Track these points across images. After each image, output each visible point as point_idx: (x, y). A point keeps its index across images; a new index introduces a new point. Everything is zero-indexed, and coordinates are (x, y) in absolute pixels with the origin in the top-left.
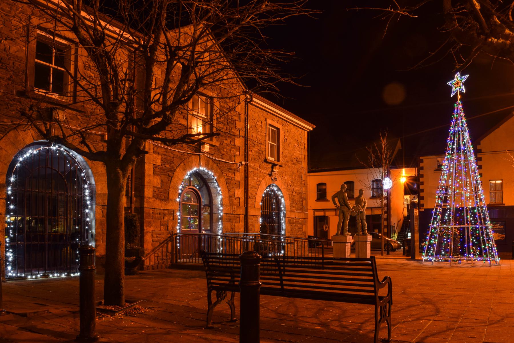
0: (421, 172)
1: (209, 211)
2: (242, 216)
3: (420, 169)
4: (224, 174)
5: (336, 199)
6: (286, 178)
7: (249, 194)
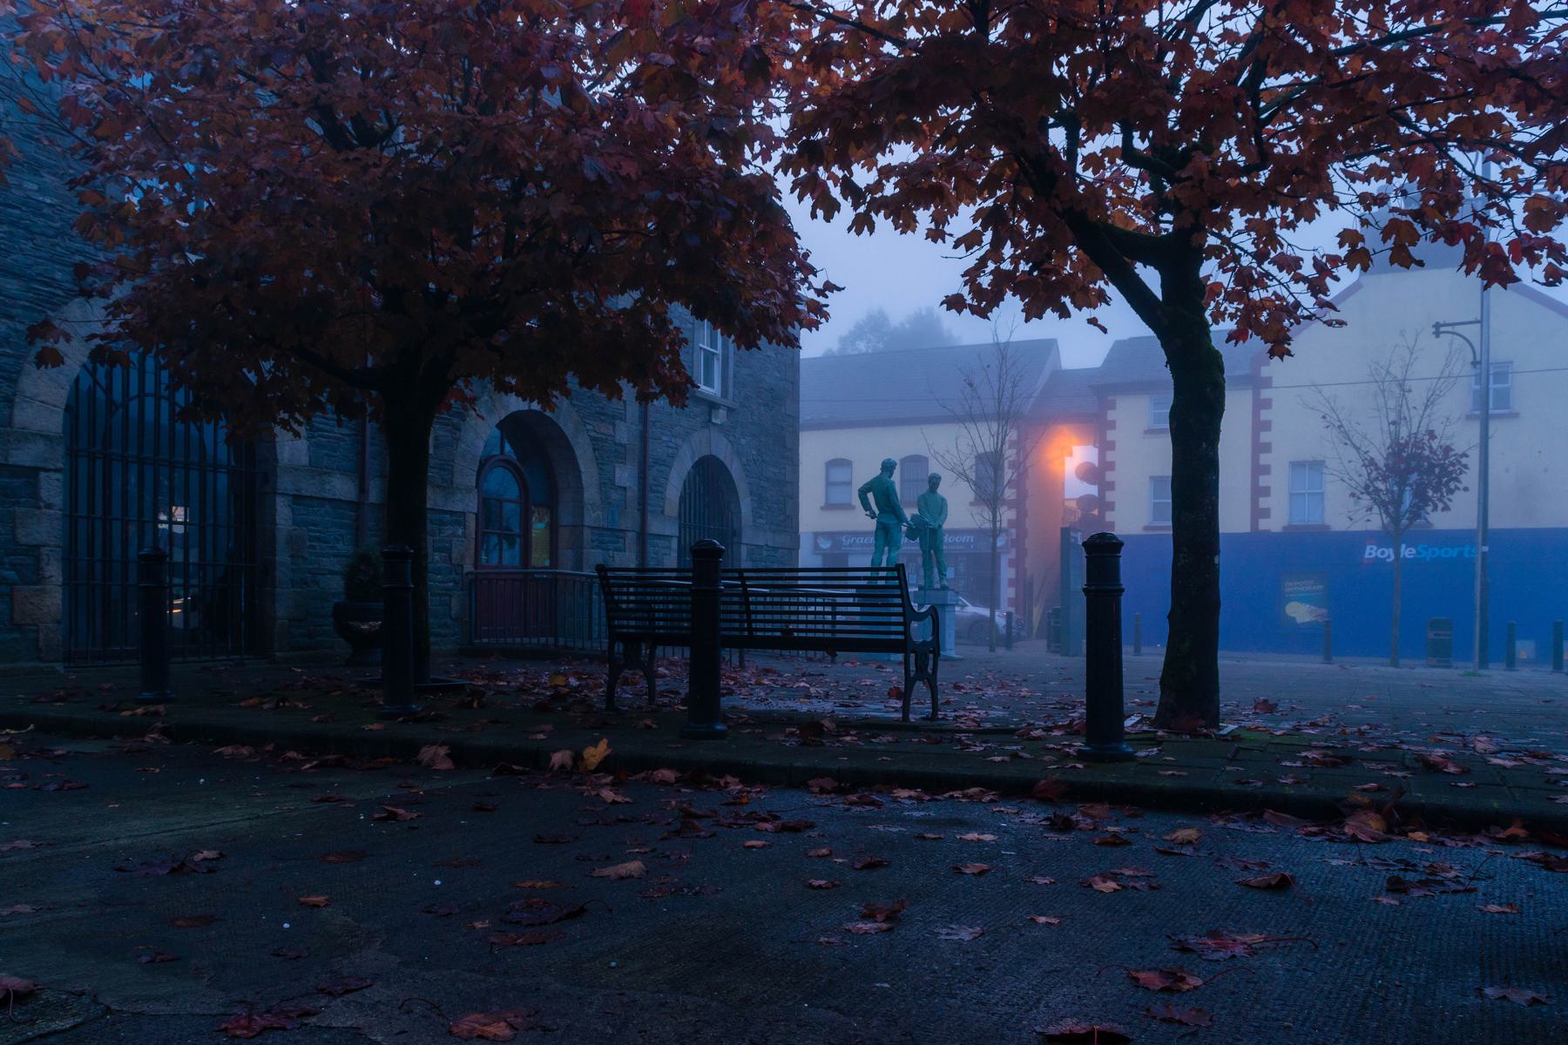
0: (1110, 456)
1: (547, 519)
2: (631, 537)
3: (1105, 446)
5: (870, 496)
6: (743, 441)
7: (650, 481)
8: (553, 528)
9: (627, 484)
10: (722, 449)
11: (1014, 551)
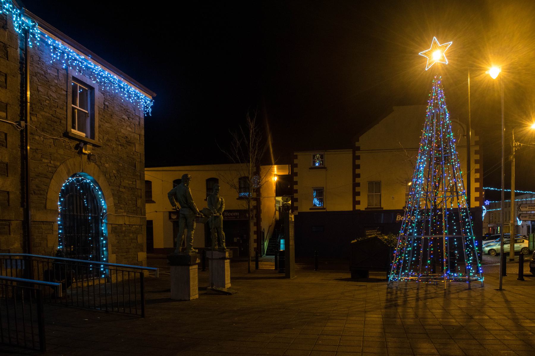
6: (107, 165)
9: (10, 189)
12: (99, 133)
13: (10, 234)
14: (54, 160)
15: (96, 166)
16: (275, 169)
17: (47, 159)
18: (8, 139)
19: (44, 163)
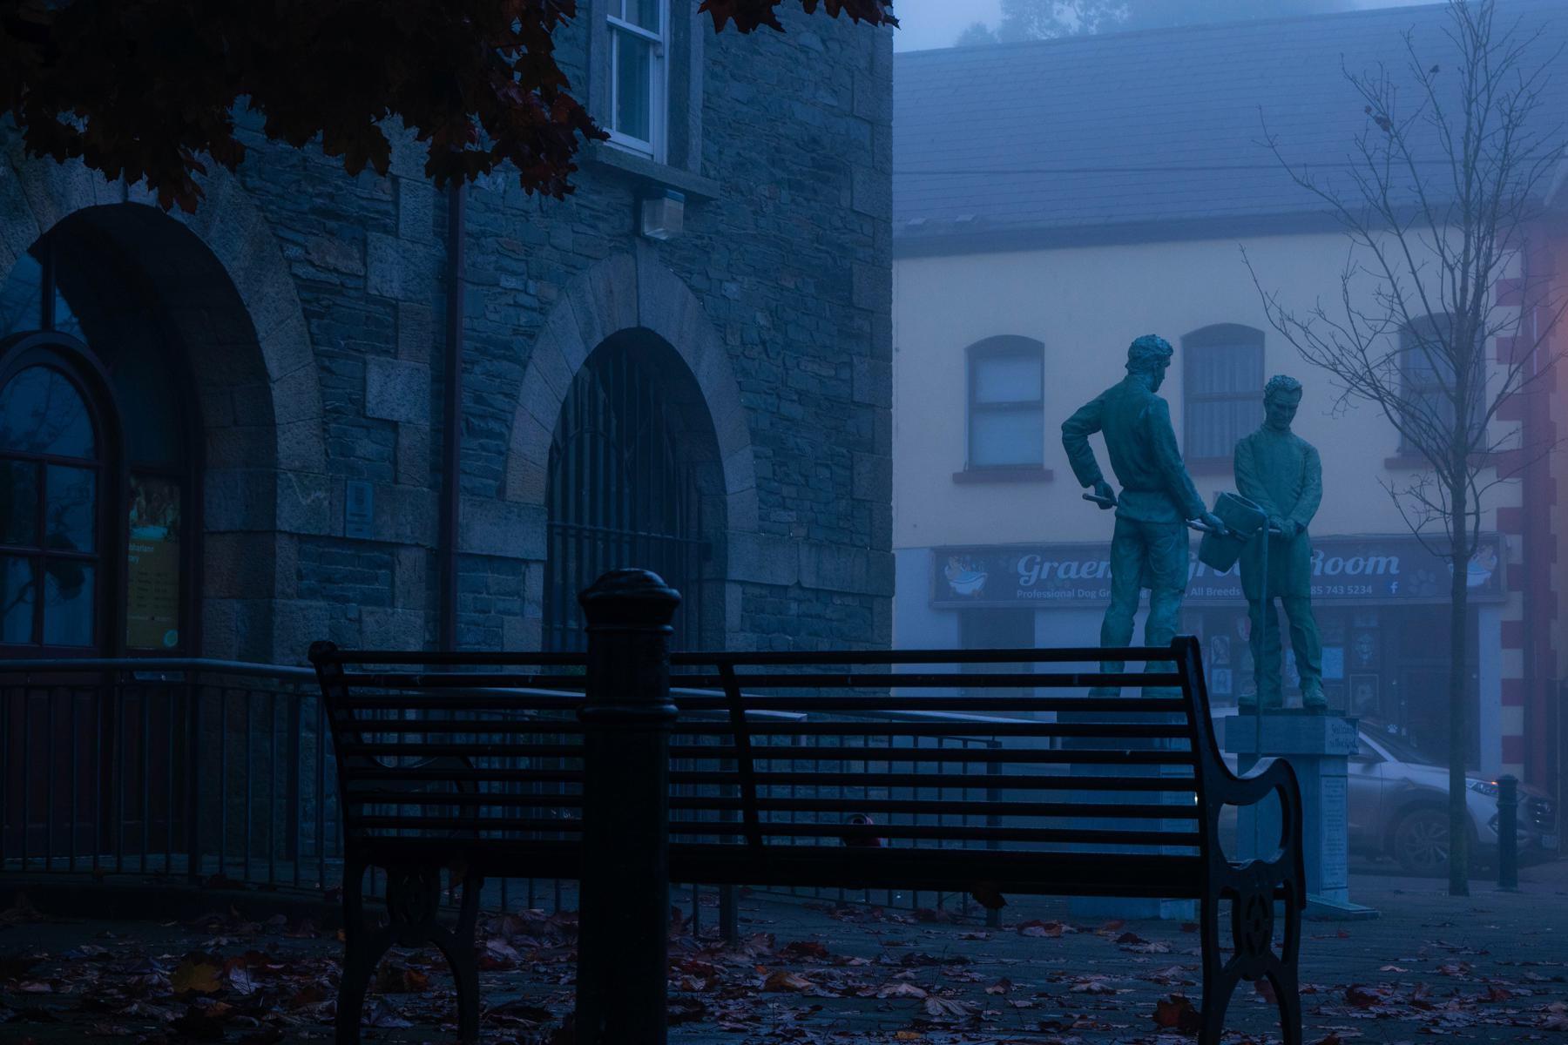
1: (171, 515)
4: (293, 251)
6: (732, 289)
8: (190, 538)
9: (401, 414)
10: (670, 310)
11: (1517, 598)
12: (706, 134)
13: (392, 605)
14: (539, 278)
15: (691, 296)
16: (671, 840)
17: (514, 273)
18: (402, 203)
19: (507, 291)
